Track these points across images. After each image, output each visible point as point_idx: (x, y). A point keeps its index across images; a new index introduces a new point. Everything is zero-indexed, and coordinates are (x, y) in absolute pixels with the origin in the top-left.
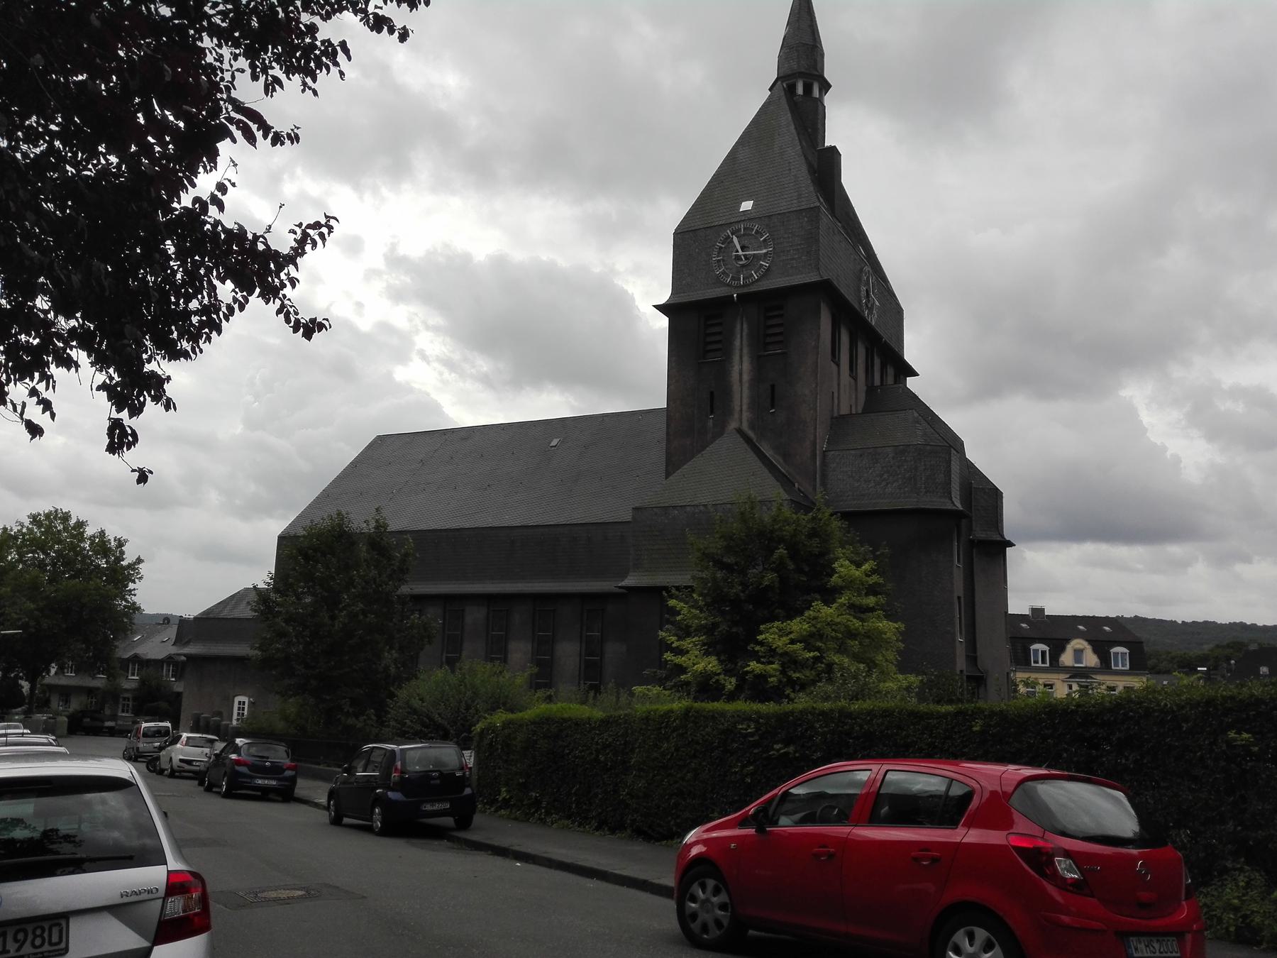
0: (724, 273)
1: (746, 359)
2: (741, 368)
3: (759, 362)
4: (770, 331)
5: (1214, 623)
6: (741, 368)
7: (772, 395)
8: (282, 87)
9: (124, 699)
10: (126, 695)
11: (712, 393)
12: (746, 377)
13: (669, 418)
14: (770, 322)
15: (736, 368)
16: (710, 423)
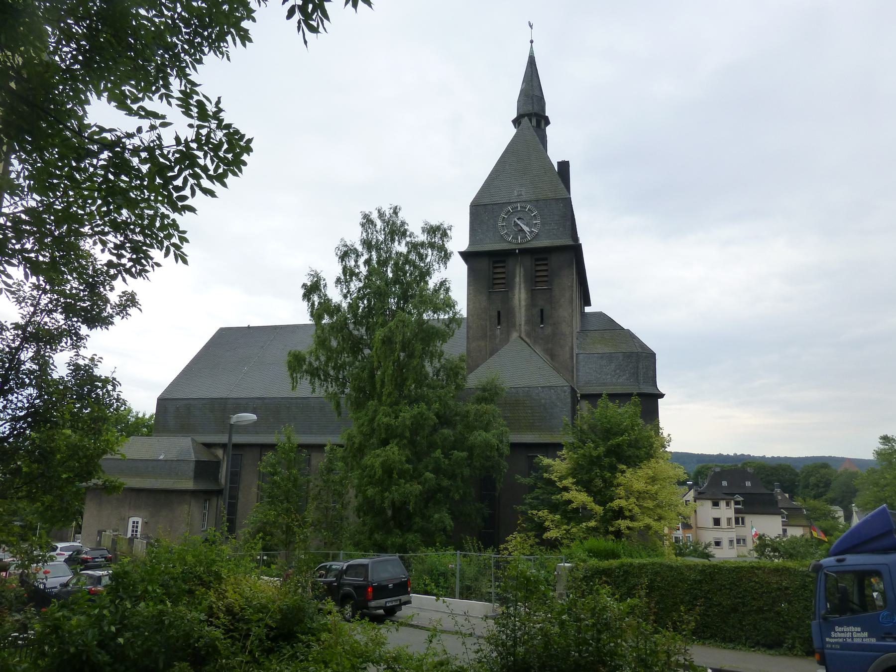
1: (523, 291)
2: (520, 296)
3: (533, 294)
5: (720, 455)
6: (520, 296)
7: (541, 316)
11: (499, 313)
12: (523, 303)
14: (539, 268)
15: (517, 297)
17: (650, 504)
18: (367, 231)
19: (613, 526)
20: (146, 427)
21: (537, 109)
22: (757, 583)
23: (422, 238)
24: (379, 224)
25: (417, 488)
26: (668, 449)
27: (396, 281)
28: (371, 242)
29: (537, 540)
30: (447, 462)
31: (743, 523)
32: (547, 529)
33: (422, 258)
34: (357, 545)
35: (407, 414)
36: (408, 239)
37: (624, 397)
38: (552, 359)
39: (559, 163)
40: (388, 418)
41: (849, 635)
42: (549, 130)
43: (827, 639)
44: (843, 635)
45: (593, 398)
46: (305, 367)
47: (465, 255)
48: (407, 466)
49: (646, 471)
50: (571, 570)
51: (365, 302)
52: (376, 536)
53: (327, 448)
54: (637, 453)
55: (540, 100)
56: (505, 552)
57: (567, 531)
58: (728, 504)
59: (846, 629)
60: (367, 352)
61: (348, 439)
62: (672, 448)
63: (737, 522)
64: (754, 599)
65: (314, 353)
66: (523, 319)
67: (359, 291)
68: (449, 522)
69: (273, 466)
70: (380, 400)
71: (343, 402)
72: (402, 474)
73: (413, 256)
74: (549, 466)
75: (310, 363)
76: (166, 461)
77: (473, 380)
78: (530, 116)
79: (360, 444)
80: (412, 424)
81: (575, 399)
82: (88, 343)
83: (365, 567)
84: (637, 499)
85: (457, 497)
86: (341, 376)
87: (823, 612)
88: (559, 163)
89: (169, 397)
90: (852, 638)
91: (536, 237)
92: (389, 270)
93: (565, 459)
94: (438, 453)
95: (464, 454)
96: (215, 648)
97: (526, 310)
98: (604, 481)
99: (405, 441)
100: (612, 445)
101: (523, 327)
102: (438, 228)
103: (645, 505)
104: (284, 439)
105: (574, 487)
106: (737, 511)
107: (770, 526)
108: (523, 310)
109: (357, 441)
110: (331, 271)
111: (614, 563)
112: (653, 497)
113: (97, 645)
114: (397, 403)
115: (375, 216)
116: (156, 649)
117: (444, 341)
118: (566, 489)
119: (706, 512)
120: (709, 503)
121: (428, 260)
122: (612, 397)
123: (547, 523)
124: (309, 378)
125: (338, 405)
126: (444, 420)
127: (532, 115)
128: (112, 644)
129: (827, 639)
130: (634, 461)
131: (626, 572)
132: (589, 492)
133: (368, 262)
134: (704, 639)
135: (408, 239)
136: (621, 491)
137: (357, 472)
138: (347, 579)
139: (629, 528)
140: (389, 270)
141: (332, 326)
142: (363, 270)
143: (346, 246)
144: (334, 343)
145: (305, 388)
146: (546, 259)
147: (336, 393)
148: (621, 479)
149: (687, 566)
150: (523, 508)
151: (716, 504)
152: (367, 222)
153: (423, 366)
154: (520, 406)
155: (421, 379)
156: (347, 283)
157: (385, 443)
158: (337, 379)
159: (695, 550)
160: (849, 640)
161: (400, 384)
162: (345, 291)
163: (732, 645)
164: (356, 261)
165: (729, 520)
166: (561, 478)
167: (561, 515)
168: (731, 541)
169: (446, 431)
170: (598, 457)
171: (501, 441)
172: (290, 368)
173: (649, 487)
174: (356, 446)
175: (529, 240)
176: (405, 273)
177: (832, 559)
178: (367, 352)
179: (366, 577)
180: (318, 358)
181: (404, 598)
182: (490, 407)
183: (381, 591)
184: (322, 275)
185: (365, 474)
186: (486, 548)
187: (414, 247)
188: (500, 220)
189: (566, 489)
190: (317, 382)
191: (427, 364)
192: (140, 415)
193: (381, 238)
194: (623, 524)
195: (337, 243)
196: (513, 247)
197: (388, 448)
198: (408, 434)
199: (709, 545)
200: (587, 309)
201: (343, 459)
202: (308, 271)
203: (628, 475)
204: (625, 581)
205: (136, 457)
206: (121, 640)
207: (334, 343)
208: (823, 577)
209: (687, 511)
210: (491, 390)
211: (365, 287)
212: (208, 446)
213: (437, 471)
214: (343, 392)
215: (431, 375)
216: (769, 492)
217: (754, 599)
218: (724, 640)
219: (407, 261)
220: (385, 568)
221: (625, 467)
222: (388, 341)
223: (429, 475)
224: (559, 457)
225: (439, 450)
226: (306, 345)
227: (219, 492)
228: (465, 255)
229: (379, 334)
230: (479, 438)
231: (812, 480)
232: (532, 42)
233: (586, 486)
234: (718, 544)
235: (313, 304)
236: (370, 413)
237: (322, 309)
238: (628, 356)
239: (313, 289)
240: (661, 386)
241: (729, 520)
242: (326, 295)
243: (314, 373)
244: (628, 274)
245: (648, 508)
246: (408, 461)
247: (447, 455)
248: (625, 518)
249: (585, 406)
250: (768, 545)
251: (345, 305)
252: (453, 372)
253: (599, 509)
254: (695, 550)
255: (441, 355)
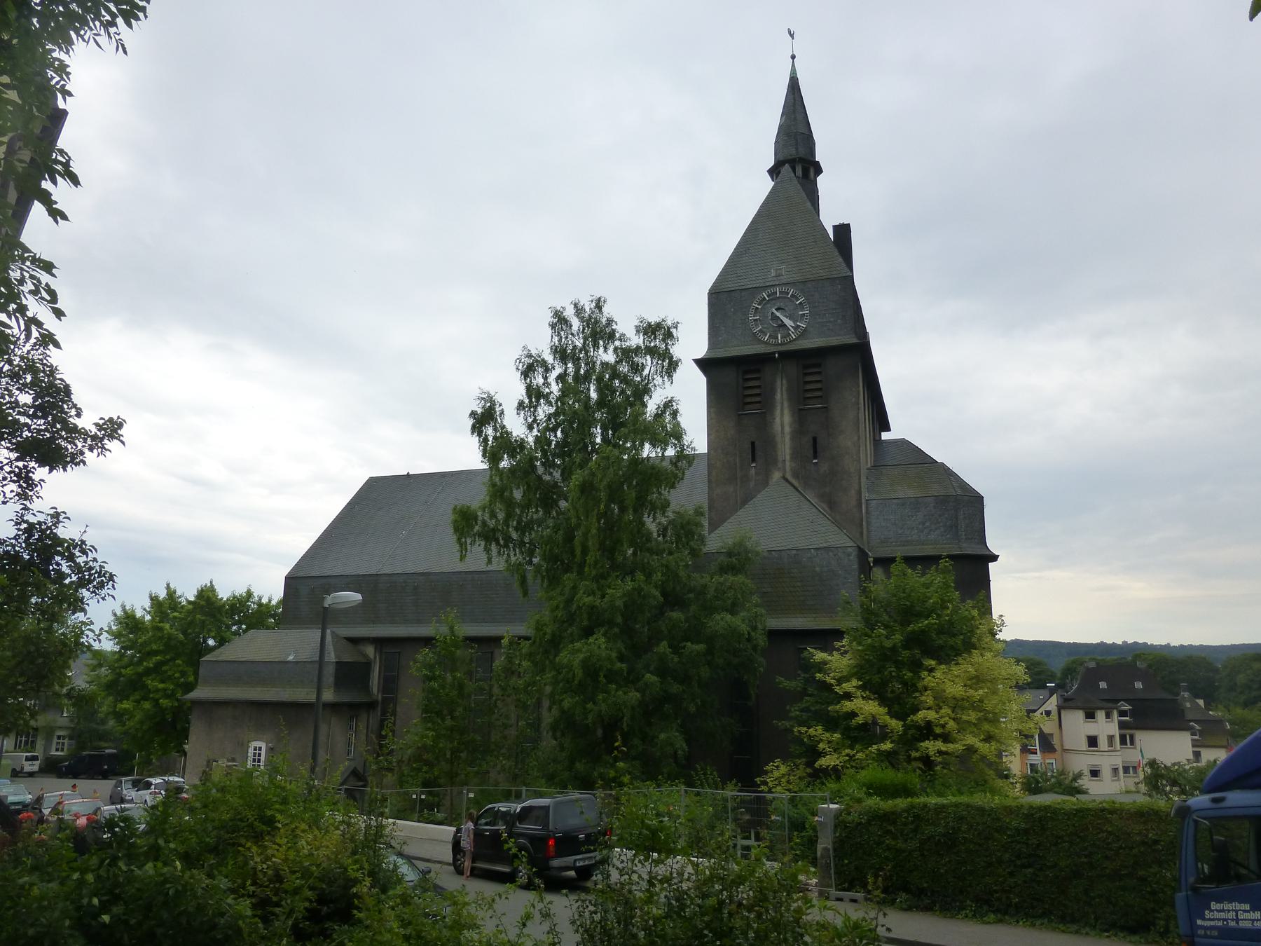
0: (760, 331)
1: (786, 412)
2: (783, 420)
3: (801, 416)
4: (808, 387)
5: (1102, 645)
6: (783, 420)
7: (813, 447)
8: (57, 345)
9: (59, 737)
10: (61, 733)
11: (753, 444)
12: (787, 429)
13: (710, 467)
14: (809, 379)
15: (778, 420)
16: (753, 471)
17: (972, 716)
18: (559, 334)
19: (917, 750)
20: (273, 616)
21: (802, 152)
22: (1110, 833)
23: (636, 340)
24: (576, 324)
25: (634, 696)
26: (1000, 636)
27: (601, 403)
28: (565, 350)
29: (809, 770)
30: (676, 659)
31: (1132, 743)
32: (821, 754)
33: (637, 369)
34: (551, 779)
35: (619, 590)
36: (617, 343)
37: (928, 561)
38: (831, 508)
39: (835, 227)
40: (591, 598)
41: (1231, 915)
42: (820, 180)
43: (1199, 922)
44: (1222, 915)
45: (885, 562)
46: (477, 528)
47: (702, 364)
48: (619, 665)
49: (966, 666)
50: (838, 814)
51: (559, 434)
52: (578, 765)
53: (505, 642)
54: (951, 641)
55: (807, 139)
56: (763, 788)
57: (851, 757)
58: (1108, 716)
59: (1226, 906)
60: (563, 504)
61: (537, 629)
62: (1005, 635)
63: (1123, 740)
64: (1107, 857)
65: (490, 508)
66: (788, 451)
67: (549, 419)
68: (681, 745)
69: (431, 667)
70: (580, 573)
71: (530, 577)
72: (611, 676)
73: (624, 368)
74: (825, 663)
75: (484, 523)
76: (297, 662)
77: (716, 541)
78: (792, 162)
79: (553, 635)
80: (625, 606)
81: (866, 564)
82: (44, 491)
83: (546, 809)
84: (953, 709)
85: (692, 709)
86: (526, 540)
87: (1191, 880)
88: (835, 227)
89: (301, 574)
90: (1237, 920)
91: (804, 334)
92: (592, 388)
93: (846, 652)
94: (663, 647)
95: (701, 647)
96: (239, 931)
97: (792, 439)
98: (905, 684)
99: (616, 630)
100: (913, 632)
101: (788, 463)
102: (659, 326)
103: (965, 718)
104: (444, 630)
105: (859, 694)
106: (1122, 725)
107: (1171, 748)
108: (787, 439)
109: (549, 631)
110: (511, 391)
111: (901, 803)
112: (977, 705)
113: (71, 927)
114: (603, 576)
115: (569, 313)
116: (159, 931)
117: (673, 486)
118: (848, 696)
119: (1076, 726)
120: (1080, 715)
121: (646, 372)
122: (911, 561)
123: (821, 746)
124: (483, 543)
125: (523, 581)
126: (672, 599)
127: (797, 160)
128: (93, 923)
129: (1199, 922)
130: (948, 655)
131: (917, 817)
132: (883, 701)
133: (561, 378)
134: (1033, 917)
135: (617, 343)
136: (928, 698)
137: (549, 675)
138: (522, 827)
139: (940, 753)
140: (592, 388)
141: (512, 470)
142: (555, 389)
143: (530, 356)
144: (518, 495)
145: (477, 558)
146: (819, 365)
147: (520, 564)
148: (928, 680)
149: (1005, 808)
150: (787, 724)
151: (1090, 715)
152: (560, 321)
153: (643, 524)
154: (782, 576)
155: (641, 539)
156: (533, 407)
157: (588, 632)
158: (522, 543)
159: (1059, 783)
160: (1232, 924)
161: (610, 549)
162: (530, 420)
163: (1075, 927)
164: (546, 378)
165: (1111, 738)
166: (840, 681)
167: (842, 734)
168: (1115, 770)
169: (676, 615)
170: (893, 649)
171: (754, 628)
172: (456, 530)
173: (971, 692)
174: (548, 637)
175: (795, 336)
176: (613, 391)
177: (1207, 797)
178: (563, 504)
179: (546, 826)
180: (493, 515)
181: (598, 856)
182: (740, 578)
183: (569, 843)
184: (497, 398)
185: (561, 677)
186: (724, 783)
187: (626, 354)
188: (752, 311)
189: (848, 696)
190: (493, 546)
191: (648, 520)
192: (265, 601)
193: (579, 343)
194: (932, 746)
195: (518, 352)
196: (772, 349)
197: (591, 640)
198: (619, 620)
199: (1079, 775)
200: (885, 436)
201: (530, 656)
202: (477, 393)
203: (938, 674)
204: (915, 831)
205: (257, 658)
206: (106, 918)
207: (518, 495)
208: (1192, 823)
209: (1049, 727)
210: (739, 554)
211: (556, 414)
212: (354, 641)
213: (662, 672)
214: (530, 562)
215: (655, 535)
216: (1170, 697)
217: (1107, 857)
218: (1063, 919)
219: (615, 374)
220: (570, 808)
221: (933, 663)
222: (587, 488)
223: (650, 678)
224: (838, 650)
225: (665, 643)
226: (477, 498)
227: (371, 706)
228: (702, 364)
229: (577, 477)
230: (722, 623)
231: (1241, 678)
232: (793, 57)
233: (877, 691)
234: (1095, 773)
235: (486, 440)
236: (567, 590)
237: (499, 446)
238: (942, 501)
239: (485, 418)
240: (993, 544)
241: (1111, 738)
242: (503, 427)
243: (489, 536)
244: (945, 380)
245: (968, 722)
246: (621, 658)
247: (676, 649)
248: (936, 737)
249: (878, 573)
250: (1162, 776)
251: (531, 439)
252: (685, 531)
253: (895, 725)
254: (1059, 783)
255: (665, 506)
